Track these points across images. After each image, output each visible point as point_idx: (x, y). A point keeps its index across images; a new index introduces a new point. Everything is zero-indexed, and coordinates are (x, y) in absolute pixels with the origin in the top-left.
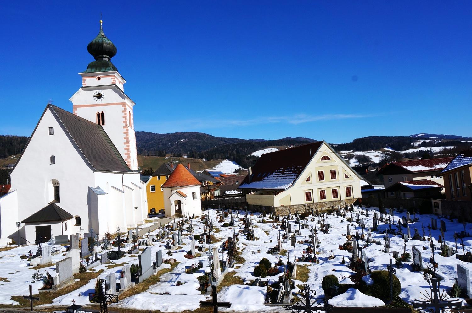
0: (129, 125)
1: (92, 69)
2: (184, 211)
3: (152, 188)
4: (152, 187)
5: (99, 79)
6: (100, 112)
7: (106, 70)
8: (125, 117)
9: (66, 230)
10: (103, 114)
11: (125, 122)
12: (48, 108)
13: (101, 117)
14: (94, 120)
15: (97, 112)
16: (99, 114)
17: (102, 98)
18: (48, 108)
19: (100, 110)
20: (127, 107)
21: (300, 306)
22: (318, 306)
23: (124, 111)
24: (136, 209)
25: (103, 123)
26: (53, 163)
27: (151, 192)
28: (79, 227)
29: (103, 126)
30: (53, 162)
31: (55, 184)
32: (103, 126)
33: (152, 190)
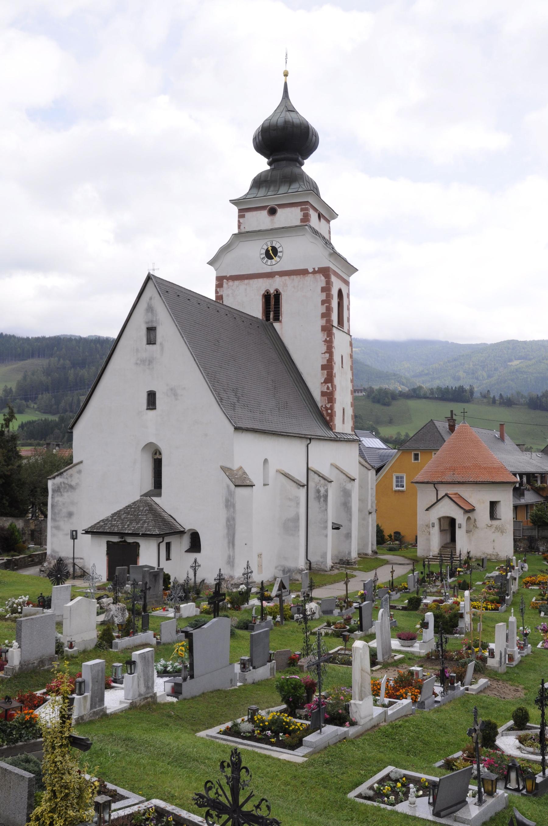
0: (335, 323)
1: (261, 189)
2: (464, 544)
3: (397, 482)
4: (397, 478)
5: (272, 212)
6: (272, 291)
7: (290, 191)
8: (327, 301)
9: (168, 558)
10: (278, 296)
11: (327, 315)
12: (212, 296)
13: (272, 303)
14: (256, 310)
15: (263, 292)
16: (270, 295)
17: (264, 256)
18: (212, 296)
19: (272, 285)
20: (333, 279)
21: (220, 803)
22: (254, 812)
23: (327, 289)
24: (338, 528)
25: (277, 318)
26: (151, 407)
27: (396, 491)
28: (193, 556)
29: (276, 325)
30: (152, 405)
31: (156, 454)
32: (276, 325)
33: (397, 486)
